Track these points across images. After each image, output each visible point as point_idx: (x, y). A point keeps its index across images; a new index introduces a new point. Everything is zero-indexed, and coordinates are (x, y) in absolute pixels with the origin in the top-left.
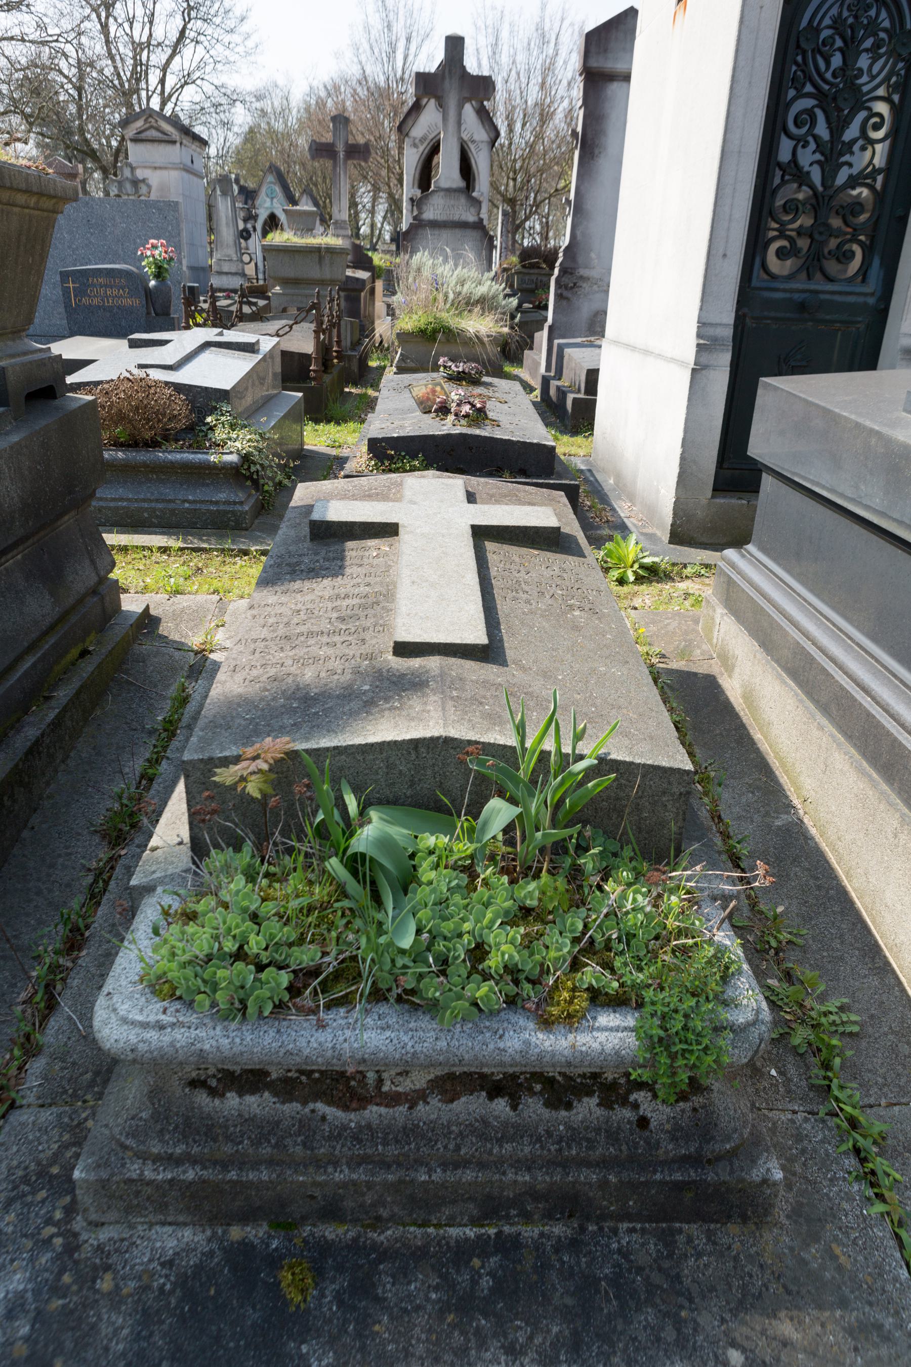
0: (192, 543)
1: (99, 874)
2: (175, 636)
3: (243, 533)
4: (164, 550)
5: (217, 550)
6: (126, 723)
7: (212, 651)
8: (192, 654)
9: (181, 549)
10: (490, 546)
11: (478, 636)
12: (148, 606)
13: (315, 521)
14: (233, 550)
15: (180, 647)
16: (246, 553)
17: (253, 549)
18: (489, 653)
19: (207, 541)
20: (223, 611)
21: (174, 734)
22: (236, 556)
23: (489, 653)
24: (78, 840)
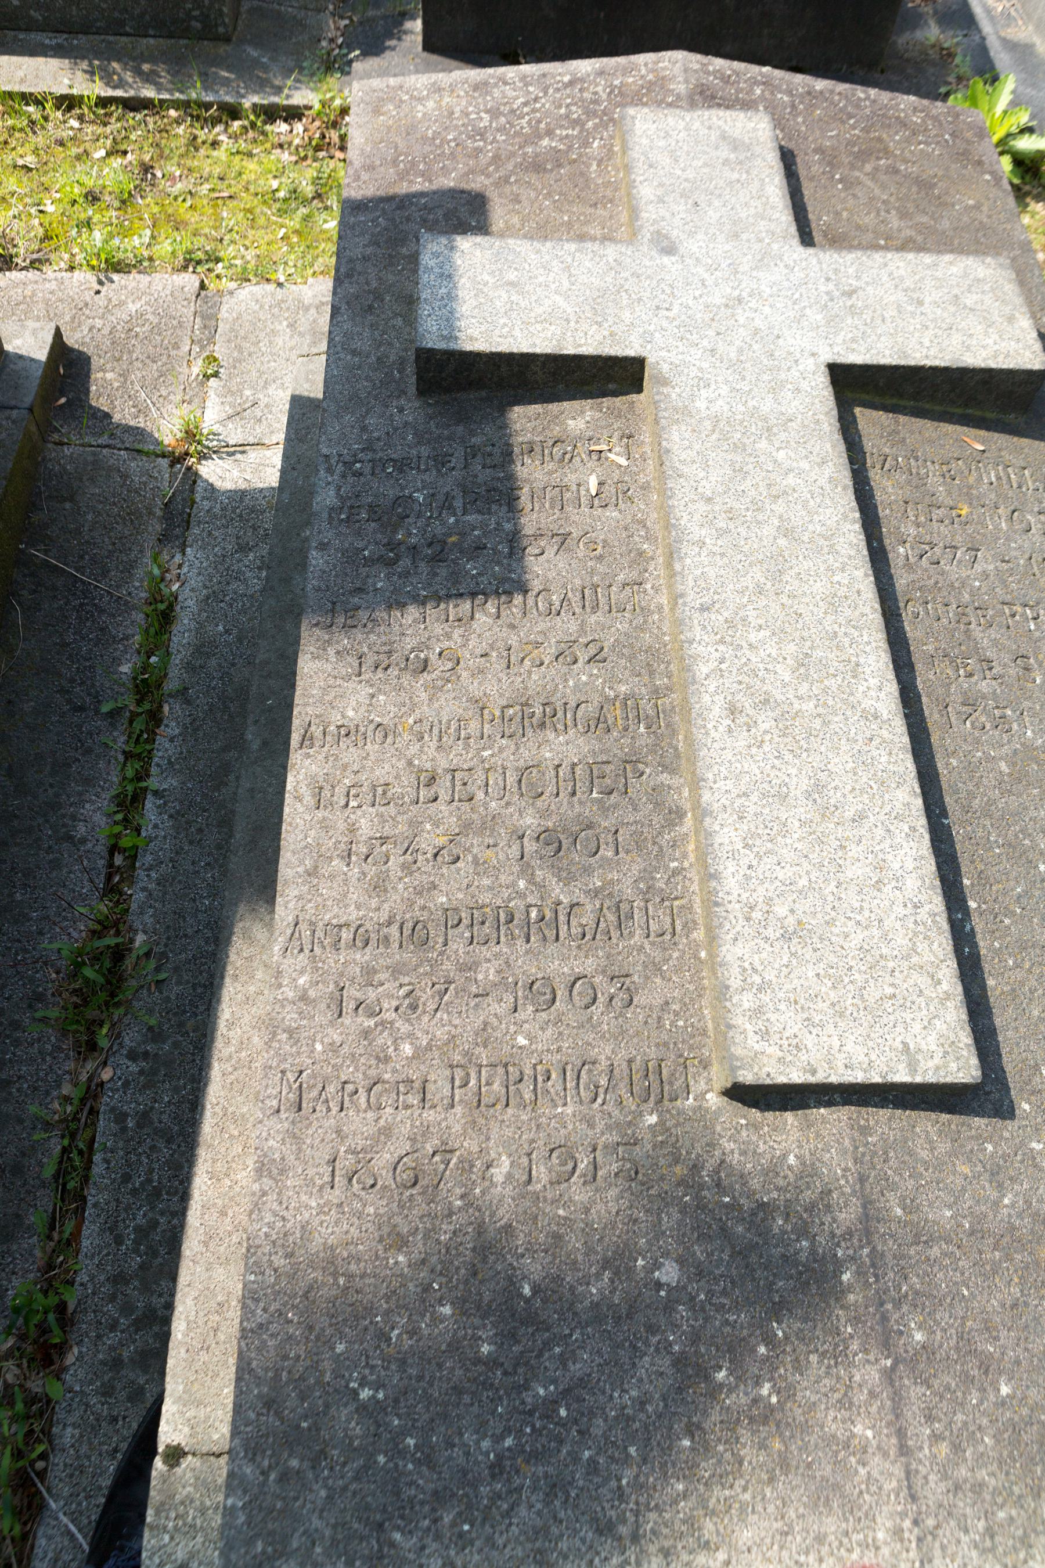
0: (121, 84)
1: (70, 1128)
2: (123, 415)
3: (223, 49)
4: (68, 103)
5: (176, 105)
6: (62, 691)
7: (202, 457)
8: (164, 463)
9: (103, 102)
10: (867, 419)
11: (962, 1068)
12: (58, 334)
13: (431, 351)
14: (208, 106)
15: (138, 442)
16: (233, 112)
17: (247, 104)
18: (982, 1097)
19: (149, 78)
20: (210, 321)
21: (155, 718)
22: (215, 121)
23: (982, 1097)
24: (17, 1043)
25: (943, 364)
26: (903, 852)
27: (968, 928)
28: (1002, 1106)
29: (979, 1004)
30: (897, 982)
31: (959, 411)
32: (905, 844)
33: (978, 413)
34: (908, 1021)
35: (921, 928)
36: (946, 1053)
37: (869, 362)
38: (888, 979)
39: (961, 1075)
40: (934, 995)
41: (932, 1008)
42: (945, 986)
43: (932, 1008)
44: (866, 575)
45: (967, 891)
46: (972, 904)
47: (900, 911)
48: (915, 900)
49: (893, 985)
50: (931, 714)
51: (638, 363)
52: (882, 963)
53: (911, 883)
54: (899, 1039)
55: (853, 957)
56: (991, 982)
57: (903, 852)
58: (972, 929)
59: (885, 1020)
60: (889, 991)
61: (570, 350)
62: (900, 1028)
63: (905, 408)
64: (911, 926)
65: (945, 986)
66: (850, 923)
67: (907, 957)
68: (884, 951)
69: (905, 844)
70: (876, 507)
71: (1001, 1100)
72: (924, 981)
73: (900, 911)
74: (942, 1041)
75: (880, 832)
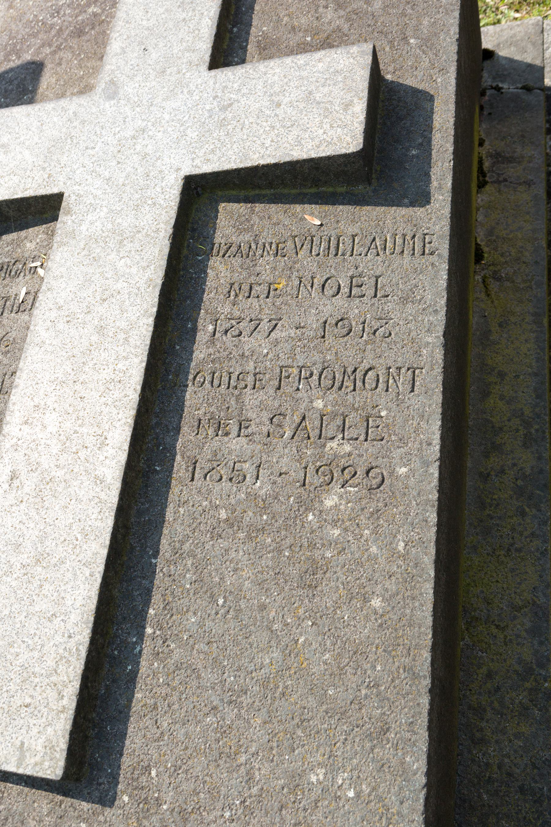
25: (273, 161)
26: (78, 592)
27: (138, 649)
28: (106, 796)
29: (121, 712)
30: (35, 694)
31: (313, 190)
32: (82, 586)
33: (331, 189)
34: (31, 725)
35: (66, 654)
36: (46, 753)
37: (216, 170)
38: (31, 692)
39: (49, 772)
40: (55, 708)
41: (50, 718)
42: (65, 702)
43: (50, 718)
44: (142, 362)
45: (149, 620)
46: (149, 630)
47: (58, 639)
48: (71, 631)
49: (32, 697)
50: (178, 471)
51: (58, 198)
52: (32, 679)
53: (74, 617)
54: (20, 738)
55: (15, 672)
56: (138, 695)
57: (78, 592)
58: (140, 652)
59: (16, 723)
60: (28, 700)
61: (19, 195)
62: (23, 731)
63: (264, 196)
64: (61, 651)
65: (65, 702)
66: (23, 646)
67: (48, 677)
68: (37, 669)
69: (82, 586)
70: (204, 291)
71: (108, 791)
72: (52, 694)
73: (58, 639)
74: (46, 744)
75: (69, 575)
